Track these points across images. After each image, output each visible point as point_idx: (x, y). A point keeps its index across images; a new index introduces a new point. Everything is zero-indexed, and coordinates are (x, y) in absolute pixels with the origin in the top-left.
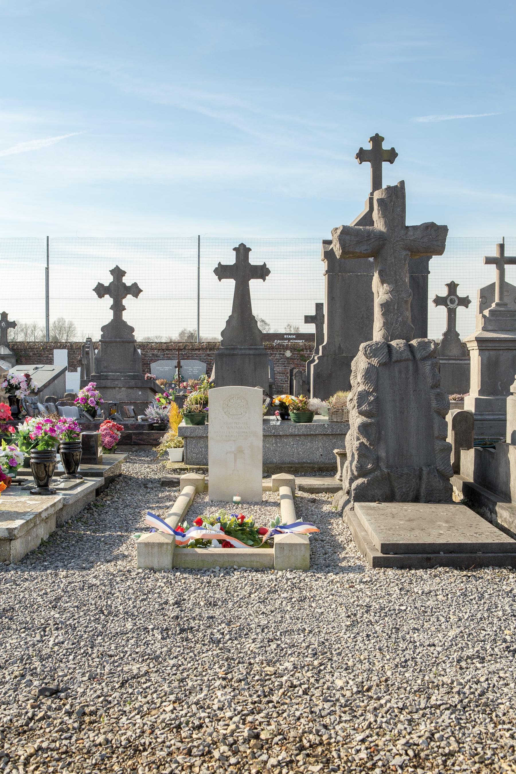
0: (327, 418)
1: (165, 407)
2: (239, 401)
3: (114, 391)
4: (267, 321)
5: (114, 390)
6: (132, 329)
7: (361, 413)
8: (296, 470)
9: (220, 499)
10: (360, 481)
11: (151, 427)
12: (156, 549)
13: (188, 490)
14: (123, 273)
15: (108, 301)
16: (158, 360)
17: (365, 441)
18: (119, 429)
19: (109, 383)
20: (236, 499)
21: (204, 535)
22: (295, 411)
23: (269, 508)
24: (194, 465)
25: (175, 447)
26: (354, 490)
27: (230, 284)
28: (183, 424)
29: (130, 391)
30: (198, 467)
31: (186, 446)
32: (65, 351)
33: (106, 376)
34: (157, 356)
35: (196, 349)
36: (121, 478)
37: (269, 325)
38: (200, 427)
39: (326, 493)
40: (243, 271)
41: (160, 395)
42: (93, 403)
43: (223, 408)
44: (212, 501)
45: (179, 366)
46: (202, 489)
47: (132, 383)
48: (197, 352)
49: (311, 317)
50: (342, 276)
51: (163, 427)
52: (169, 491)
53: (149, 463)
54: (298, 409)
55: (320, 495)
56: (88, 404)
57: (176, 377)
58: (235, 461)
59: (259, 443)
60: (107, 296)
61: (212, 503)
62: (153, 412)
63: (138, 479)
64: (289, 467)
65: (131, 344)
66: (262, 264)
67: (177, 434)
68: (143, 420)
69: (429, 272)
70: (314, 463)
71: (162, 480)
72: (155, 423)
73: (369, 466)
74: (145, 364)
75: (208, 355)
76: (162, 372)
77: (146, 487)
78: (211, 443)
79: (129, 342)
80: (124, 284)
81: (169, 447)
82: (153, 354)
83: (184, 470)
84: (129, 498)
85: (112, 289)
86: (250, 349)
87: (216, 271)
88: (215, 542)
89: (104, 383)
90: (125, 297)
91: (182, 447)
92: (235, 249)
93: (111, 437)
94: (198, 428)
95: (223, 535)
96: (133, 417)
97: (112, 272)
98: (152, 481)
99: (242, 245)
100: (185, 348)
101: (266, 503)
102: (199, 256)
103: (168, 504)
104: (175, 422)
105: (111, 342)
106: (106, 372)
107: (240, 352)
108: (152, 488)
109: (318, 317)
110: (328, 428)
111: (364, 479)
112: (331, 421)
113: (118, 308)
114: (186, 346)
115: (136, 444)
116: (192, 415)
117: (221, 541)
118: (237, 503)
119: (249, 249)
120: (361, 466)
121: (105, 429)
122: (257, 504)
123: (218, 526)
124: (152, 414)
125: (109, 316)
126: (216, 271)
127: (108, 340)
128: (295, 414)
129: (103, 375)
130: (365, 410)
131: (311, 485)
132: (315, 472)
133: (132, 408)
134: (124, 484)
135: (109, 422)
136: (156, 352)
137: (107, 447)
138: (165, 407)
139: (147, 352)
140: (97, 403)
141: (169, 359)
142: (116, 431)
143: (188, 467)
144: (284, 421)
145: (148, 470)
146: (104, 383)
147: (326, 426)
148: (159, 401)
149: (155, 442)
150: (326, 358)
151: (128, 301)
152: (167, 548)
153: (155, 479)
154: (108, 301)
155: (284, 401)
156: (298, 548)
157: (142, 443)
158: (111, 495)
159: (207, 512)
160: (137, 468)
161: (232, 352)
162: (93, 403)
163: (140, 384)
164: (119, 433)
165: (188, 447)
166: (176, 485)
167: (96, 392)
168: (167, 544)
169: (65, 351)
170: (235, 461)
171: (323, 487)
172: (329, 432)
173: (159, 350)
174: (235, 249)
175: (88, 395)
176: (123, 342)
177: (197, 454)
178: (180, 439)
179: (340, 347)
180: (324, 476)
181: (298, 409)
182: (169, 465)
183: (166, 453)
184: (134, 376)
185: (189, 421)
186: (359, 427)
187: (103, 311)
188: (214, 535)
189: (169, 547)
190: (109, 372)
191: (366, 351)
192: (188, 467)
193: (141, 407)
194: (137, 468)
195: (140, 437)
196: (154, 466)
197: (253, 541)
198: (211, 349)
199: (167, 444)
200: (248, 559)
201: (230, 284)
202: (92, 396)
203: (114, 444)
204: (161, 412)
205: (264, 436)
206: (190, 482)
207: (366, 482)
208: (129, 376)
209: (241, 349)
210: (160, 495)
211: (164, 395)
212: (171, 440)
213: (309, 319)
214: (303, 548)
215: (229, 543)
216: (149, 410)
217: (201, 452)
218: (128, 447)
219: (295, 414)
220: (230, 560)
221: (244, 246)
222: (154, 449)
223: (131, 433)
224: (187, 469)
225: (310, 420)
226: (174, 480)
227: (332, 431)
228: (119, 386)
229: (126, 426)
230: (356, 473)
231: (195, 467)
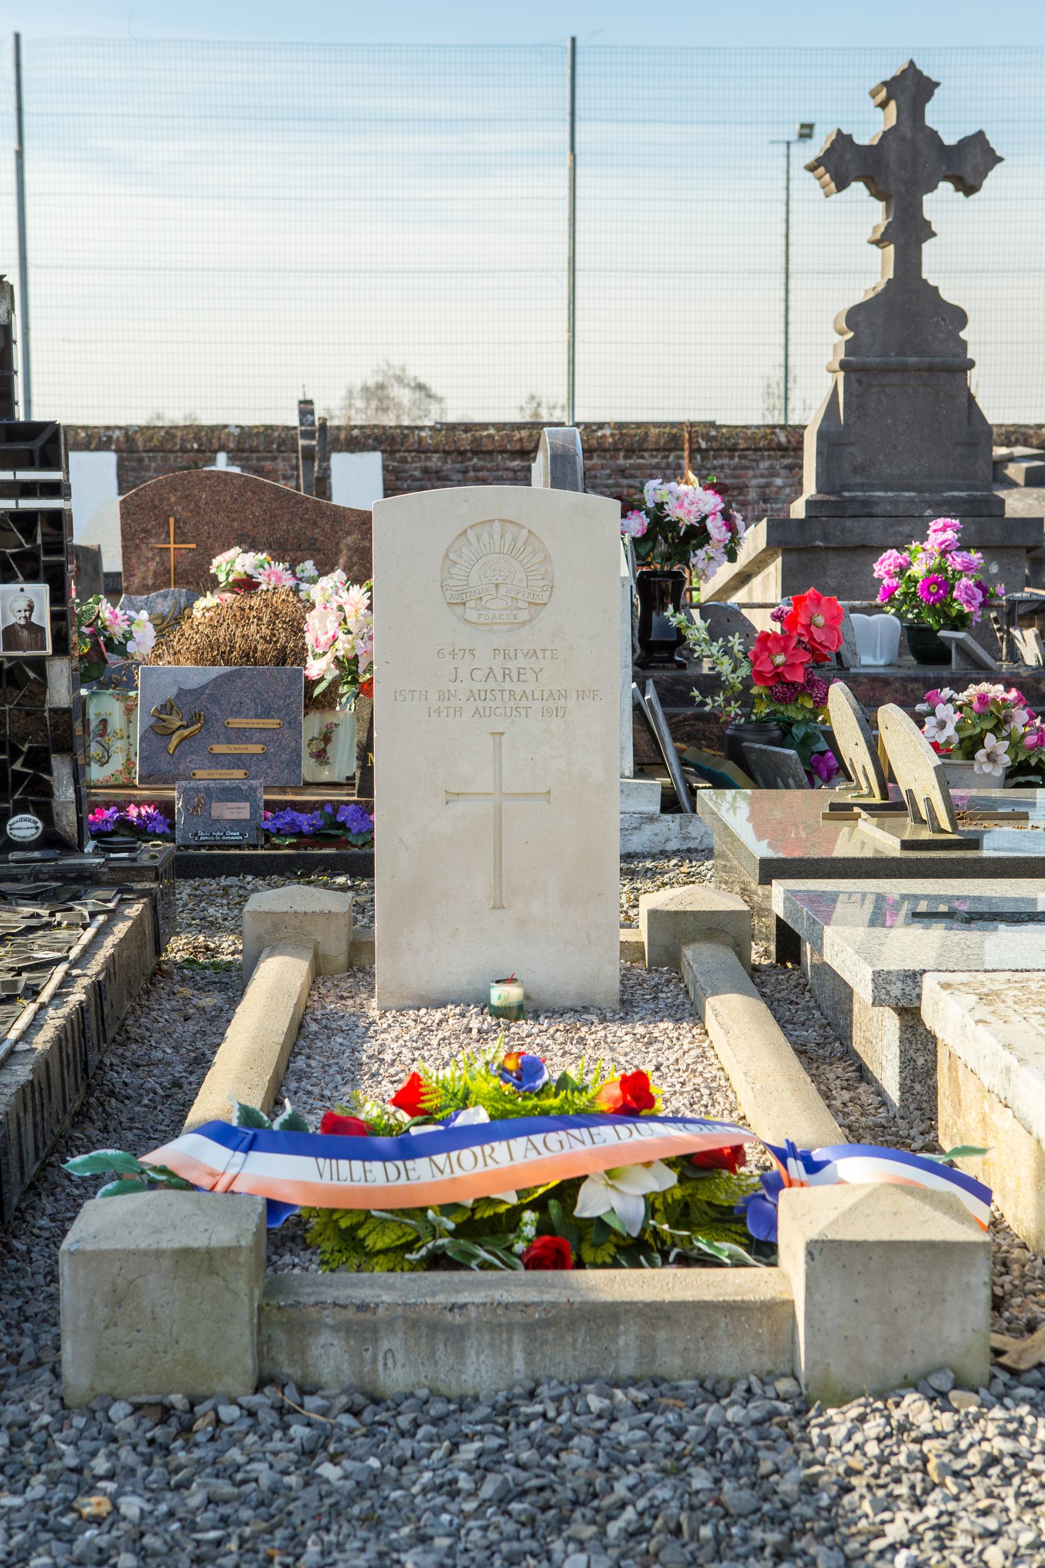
4: (436, 389)
6: (959, 318)
33: (867, 503)
37: (440, 400)
60: (858, 189)
75: (622, 472)
82: (426, 470)
90: (932, 188)
105: (884, 370)
106: (861, 487)
113: (907, 233)
125: (872, 271)
127: (873, 360)
129: (853, 500)
136: (435, 461)
139: (404, 460)
169: (108, 460)
173: (447, 453)
176: (931, 369)
184: (971, 501)
187: (845, 244)
190: (872, 487)
198: (630, 452)
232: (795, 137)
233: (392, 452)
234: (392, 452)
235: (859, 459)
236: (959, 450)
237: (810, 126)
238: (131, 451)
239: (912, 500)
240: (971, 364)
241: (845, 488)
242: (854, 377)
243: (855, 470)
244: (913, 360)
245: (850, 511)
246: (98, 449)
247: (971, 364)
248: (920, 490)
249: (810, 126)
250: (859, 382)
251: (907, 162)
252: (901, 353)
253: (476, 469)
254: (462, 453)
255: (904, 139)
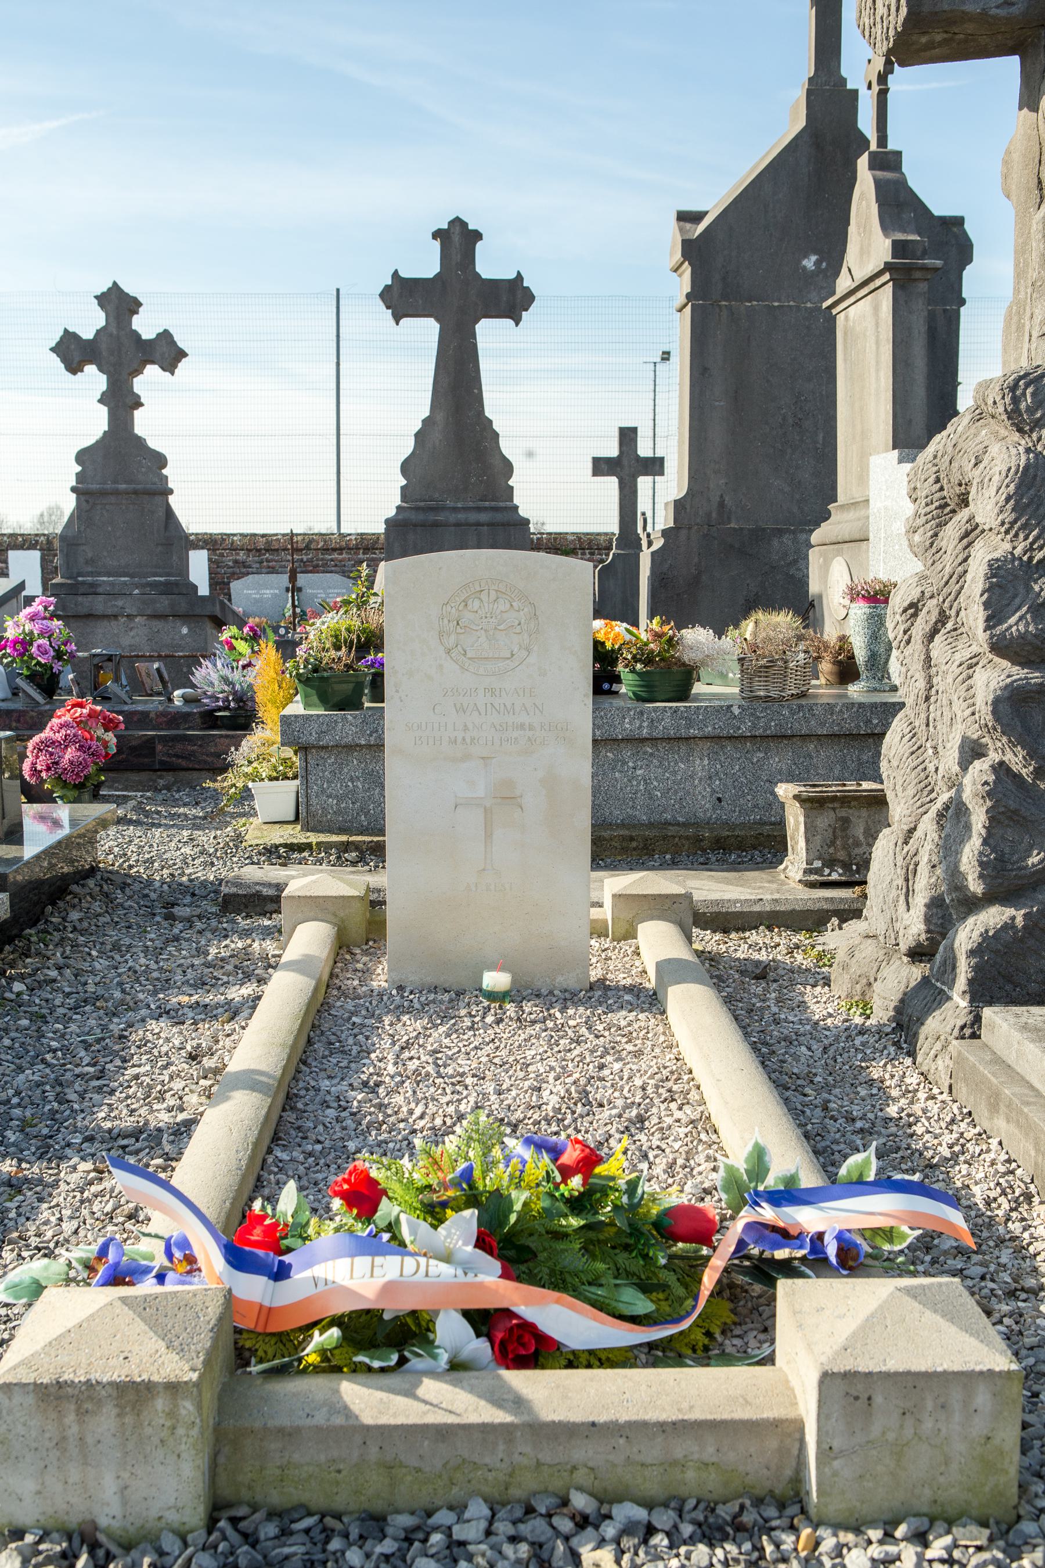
0: (737, 690)
1: (249, 665)
2: (502, 605)
3: (114, 627)
5: (113, 623)
6: (160, 461)
7: (1000, 647)
8: (645, 847)
9: (430, 980)
10: (994, 917)
11: (210, 719)
12: (105, 1422)
13: (309, 940)
14: (132, 305)
15: (94, 379)
16: (248, 574)
17: (1016, 760)
18: (109, 725)
19: (99, 605)
20: (495, 980)
21: (389, 1288)
22: (639, 666)
23: (621, 1017)
24: (331, 831)
25: (271, 779)
26: (972, 953)
27: (425, 331)
28: (296, 708)
29: (157, 625)
30: (344, 838)
31: (305, 776)
32: (36, 555)
33: (92, 585)
34: (244, 564)
35: (334, 550)
36: (91, 883)
38: (349, 714)
39: (770, 928)
40: (459, 295)
41: (234, 630)
42: (46, 653)
43: (441, 635)
44: (401, 988)
45: (295, 589)
46: (361, 930)
47: (163, 603)
48: (335, 556)
49: (608, 461)
50: (729, 308)
51: (242, 721)
52: (246, 933)
53: (197, 825)
54: (648, 661)
55: (753, 937)
56: (31, 657)
57: (289, 613)
58: (489, 836)
59: (579, 767)
60: (91, 369)
61: (404, 1000)
62: (214, 677)
63: (150, 882)
64: (623, 838)
65: (158, 499)
66: (512, 276)
67: (279, 739)
68: (187, 700)
69: (963, 302)
70: (696, 825)
71: (225, 889)
72: (220, 709)
73: (1034, 860)
74: (217, 583)
76: (256, 601)
77: (170, 917)
78: (396, 769)
79: (152, 493)
80: (136, 335)
81: (256, 777)
82: (236, 562)
83: (300, 848)
84: (101, 964)
85: (103, 346)
86: (479, 509)
87: (386, 295)
88: (452, 1332)
89: (85, 604)
90: (138, 371)
91: (295, 777)
92: (437, 234)
93: (81, 748)
94: (344, 718)
95: (491, 1283)
96: (159, 694)
97: (103, 300)
98: (194, 891)
99: (458, 223)
100: (308, 548)
101: (601, 994)
102: (338, 336)
103: (238, 993)
104: (273, 702)
105: (103, 493)
107: (452, 518)
108: (189, 922)
109: (625, 462)
110: (740, 718)
111: (1010, 912)
112: (750, 697)
113: (121, 402)
114: (310, 542)
115: (168, 768)
116: (322, 678)
117: (481, 1320)
118: (497, 997)
119: (477, 236)
120: (1001, 859)
121: (62, 726)
122: (569, 998)
123: (462, 1225)
124: (212, 684)
125: (96, 423)
126: (386, 295)
127: (95, 487)
128: (639, 674)
129: (83, 583)
130: (1022, 636)
131: (717, 902)
132: (704, 850)
133: (156, 666)
134: (97, 907)
135: (81, 705)
136: (242, 556)
137: (69, 777)
138: (249, 665)
139: (222, 555)
140: (59, 655)
141: (272, 571)
142: (100, 732)
143: (313, 838)
144: (601, 698)
145: (187, 850)
146: (85, 604)
147: (736, 711)
148: (232, 648)
149: (219, 764)
150: (684, 533)
151: (149, 381)
152: (171, 1414)
153: (204, 884)
154: (94, 379)
155: (601, 637)
156: (956, 1395)
157: (184, 763)
158: (38, 954)
159: (386, 1043)
160: (152, 844)
161: (432, 517)
162: (46, 653)
163: (183, 606)
164: (110, 737)
165: (312, 778)
166: (270, 907)
167: (56, 623)
168: (173, 1388)
169: (36, 555)
170: (489, 836)
171: (757, 908)
172: (744, 729)
173: (249, 550)
174: (437, 234)
175: (31, 633)
176: (136, 492)
177: (340, 799)
178: (288, 752)
179: (722, 504)
180: (735, 867)
181: (648, 661)
182: (257, 832)
183: (246, 795)
184: (166, 584)
185: (315, 699)
186: (996, 702)
187: (81, 409)
188: (449, 1288)
189: (187, 1407)
190: (99, 574)
191: (1016, 401)
192: (313, 838)
193: (181, 668)
194: (152, 844)
195: (179, 747)
196: (206, 838)
197: (645, 1288)
199: (249, 770)
200: (652, 1452)
201: (425, 331)
202: (42, 634)
203: (92, 769)
204: (236, 676)
205: (595, 741)
206: (317, 907)
207: (1019, 922)
208: (153, 585)
209: (455, 509)
210: (213, 951)
211: (246, 630)
212: (261, 758)
213: (604, 467)
214: (982, 1398)
215: (529, 1328)
216: (203, 671)
217: (354, 791)
218: (144, 776)
219: (639, 674)
220: (546, 1457)
221: (463, 224)
222: (209, 784)
223: (153, 737)
224: (308, 846)
225: (683, 693)
226: (266, 892)
227: (754, 726)
228: (128, 611)
229: (140, 719)
230: (975, 886)
231: (335, 838)
232: (659, 360)
233: (214, 550)
234: (214, 550)
235: (90, 555)
236: (160, 548)
237: (668, 353)
238: (49, 550)
239: (125, 583)
240: (171, 492)
241: (79, 574)
242: (83, 498)
243: (87, 563)
244: (123, 486)
245: (81, 591)
246: (28, 549)
247: (171, 492)
248: (132, 576)
249: (668, 353)
250: (87, 502)
251: (119, 349)
252: (115, 482)
253: (268, 561)
254: (259, 551)
255: (111, 335)
